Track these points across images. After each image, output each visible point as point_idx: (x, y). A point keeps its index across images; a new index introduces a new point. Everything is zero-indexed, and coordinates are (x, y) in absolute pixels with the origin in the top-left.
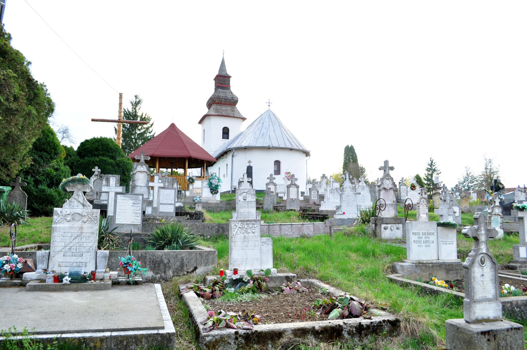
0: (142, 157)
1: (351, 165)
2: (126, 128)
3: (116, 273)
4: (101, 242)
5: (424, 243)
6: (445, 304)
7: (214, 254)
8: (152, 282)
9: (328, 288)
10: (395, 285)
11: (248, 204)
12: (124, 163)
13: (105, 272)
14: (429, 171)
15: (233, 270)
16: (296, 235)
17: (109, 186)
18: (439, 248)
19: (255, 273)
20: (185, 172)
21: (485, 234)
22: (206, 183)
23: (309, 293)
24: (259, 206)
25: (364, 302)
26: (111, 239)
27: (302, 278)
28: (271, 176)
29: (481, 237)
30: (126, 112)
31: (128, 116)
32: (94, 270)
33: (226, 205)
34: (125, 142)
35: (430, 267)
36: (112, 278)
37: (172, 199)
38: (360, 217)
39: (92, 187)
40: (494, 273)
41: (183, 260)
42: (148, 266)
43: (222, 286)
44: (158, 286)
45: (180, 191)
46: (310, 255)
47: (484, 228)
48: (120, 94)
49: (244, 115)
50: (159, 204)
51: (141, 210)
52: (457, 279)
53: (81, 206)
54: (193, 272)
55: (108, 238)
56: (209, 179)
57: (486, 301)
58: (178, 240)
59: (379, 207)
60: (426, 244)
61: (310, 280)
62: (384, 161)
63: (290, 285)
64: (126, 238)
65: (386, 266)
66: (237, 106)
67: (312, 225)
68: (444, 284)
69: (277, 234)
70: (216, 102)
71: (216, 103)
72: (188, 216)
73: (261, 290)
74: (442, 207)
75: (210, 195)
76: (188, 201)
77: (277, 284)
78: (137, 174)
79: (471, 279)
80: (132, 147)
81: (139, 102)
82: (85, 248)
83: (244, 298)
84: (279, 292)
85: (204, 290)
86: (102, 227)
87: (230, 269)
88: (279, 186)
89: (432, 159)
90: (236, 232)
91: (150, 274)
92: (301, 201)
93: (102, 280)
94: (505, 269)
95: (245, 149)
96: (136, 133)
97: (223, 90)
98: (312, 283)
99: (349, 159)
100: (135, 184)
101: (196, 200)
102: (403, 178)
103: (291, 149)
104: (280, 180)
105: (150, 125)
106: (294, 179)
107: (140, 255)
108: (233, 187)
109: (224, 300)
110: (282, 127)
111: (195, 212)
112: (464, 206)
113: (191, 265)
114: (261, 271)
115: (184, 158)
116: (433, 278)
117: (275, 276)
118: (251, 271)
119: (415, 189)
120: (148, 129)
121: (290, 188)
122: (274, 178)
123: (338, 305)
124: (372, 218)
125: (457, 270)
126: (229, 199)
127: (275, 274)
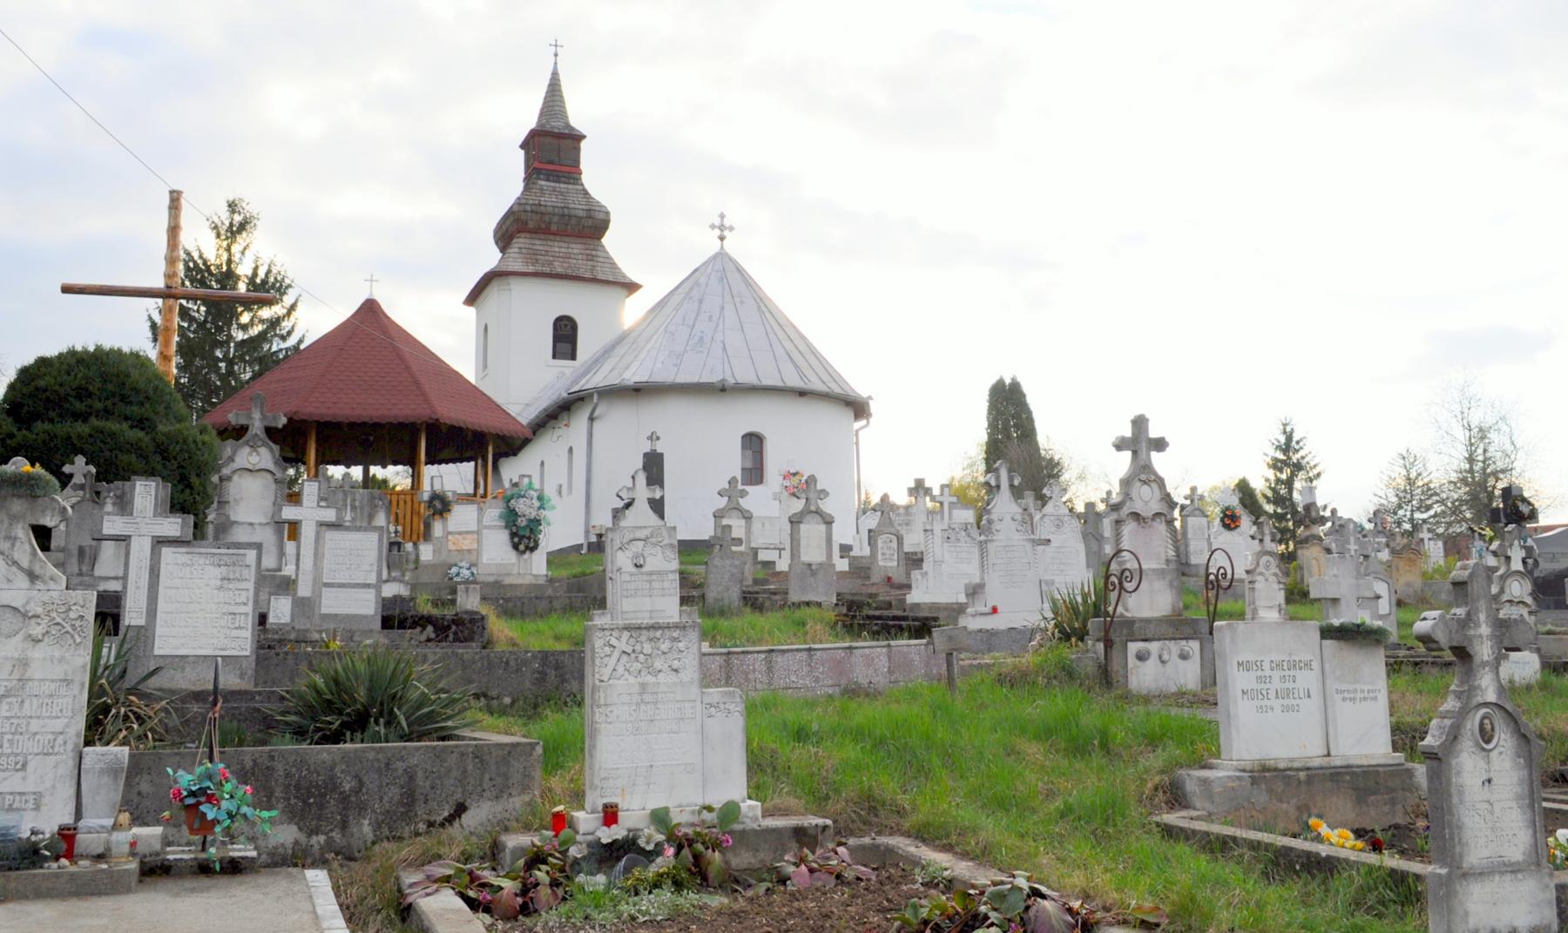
0: (257, 415)
1: (1014, 450)
2: (192, 319)
3: (158, 830)
4: (98, 723)
5: (1277, 697)
6: (1357, 904)
7: (531, 755)
8: (296, 865)
9: (947, 865)
10: (1182, 848)
11: (650, 582)
12: (185, 441)
13: (116, 827)
14: (1281, 470)
15: (600, 808)
16: (826, 687)
17: (131, 514)
18: (1330, 716)
19: (682, 818)
20: (416, 478)
21: (1492, 637)
22: (493, 512)
23: (878, 886)
24: (692, 592)
25: (1079, 903)
26: (135, 713)
27: (852, 833)
28: (733, 485)
29: (1477, 648)
30: (195, 262)
31: (203, 276)
32: (68, 819)
33: (569, 590)
34: (191, 374)
35: (1300, 782)
36: (140, 849)
37: (368, 568)
38: (1053, 622)
39: (65, 509)
40: (1526, 773)
41: (412, 778)
42: (280, 806)
43: (562, 870)
44: (318, 878)
45: (399, 544)
46: (882, 753)
47: (1487, 617)
48: (171, 192)
49: (631, 273)
50: (320, 584)
51: (251, 603)
52: (1393, 822)
53: (22, 581)
54: (451, 824)
55: (123, 710)
56: (504, 498)
57: (1502, 873)
58: (391, 712)
59: (1116, 581)
60: (1286, 702)
61: (884, 840)
62: (1132, 418)
63: (811, 857)
64: (195, 708)
65: (1150, 785)
66: (604, 240)
67: (884, 650)
68: (1351, 839)
69: (759, 686)
70: (531, 225)
71: (530, 231)
72: (430, 629)
73: (705, 878)
74: (1335, 572)
75: (511, 556)
76: (425, 578)
77: (765, 856)
78: (235, 478)
79: (1450, 796)
80: (214, 391)
81: (243, 227)
82: (37, 737)
83: (644, 908)
84: (770, 885)
85: (492, 886)
86: (100, 670)
87: (588, 806)
88: (760, 525)
89: (1288, 429)
90: (610, 669)
91: (286, 835)
92: (842, 574)
93: (100, 857)
94: (1551, 783)
95: (638, 391)
96: (230, 337)
97: (552, 184)
98: (890, 851)
99: (1006, 429)
100: (228, 517)
101: (458, 575)
102: (1193, 489)
103: (802, 394)
104: (765, 502)
105: (285, 311)
106: (816, 490)
107: (249, 764)
108: (591, 530)
109: (568, 918)
110: (768, 315)
111: (456, 615)
112: (1402, 581)
113: (444, 795)
114: (705, 812)
115: (413, 425)
116: (1312, 821)
117: (755, 826)
118: (666, 810)
119: (1237, 527)
120: (274, 323)
121: (801, 525)
122: (743, 494)
123: (986, 917)
124: (1093, 624)
125: (1393, 790)
126: (578, 570)
127: (757, 819)
